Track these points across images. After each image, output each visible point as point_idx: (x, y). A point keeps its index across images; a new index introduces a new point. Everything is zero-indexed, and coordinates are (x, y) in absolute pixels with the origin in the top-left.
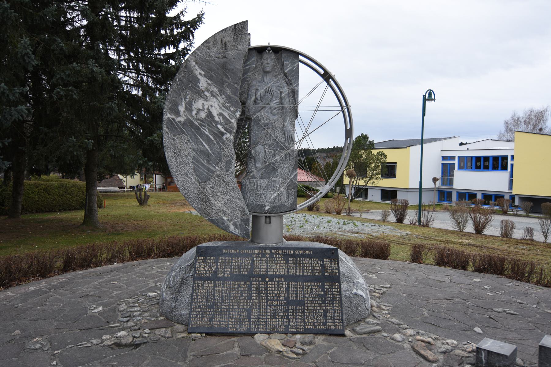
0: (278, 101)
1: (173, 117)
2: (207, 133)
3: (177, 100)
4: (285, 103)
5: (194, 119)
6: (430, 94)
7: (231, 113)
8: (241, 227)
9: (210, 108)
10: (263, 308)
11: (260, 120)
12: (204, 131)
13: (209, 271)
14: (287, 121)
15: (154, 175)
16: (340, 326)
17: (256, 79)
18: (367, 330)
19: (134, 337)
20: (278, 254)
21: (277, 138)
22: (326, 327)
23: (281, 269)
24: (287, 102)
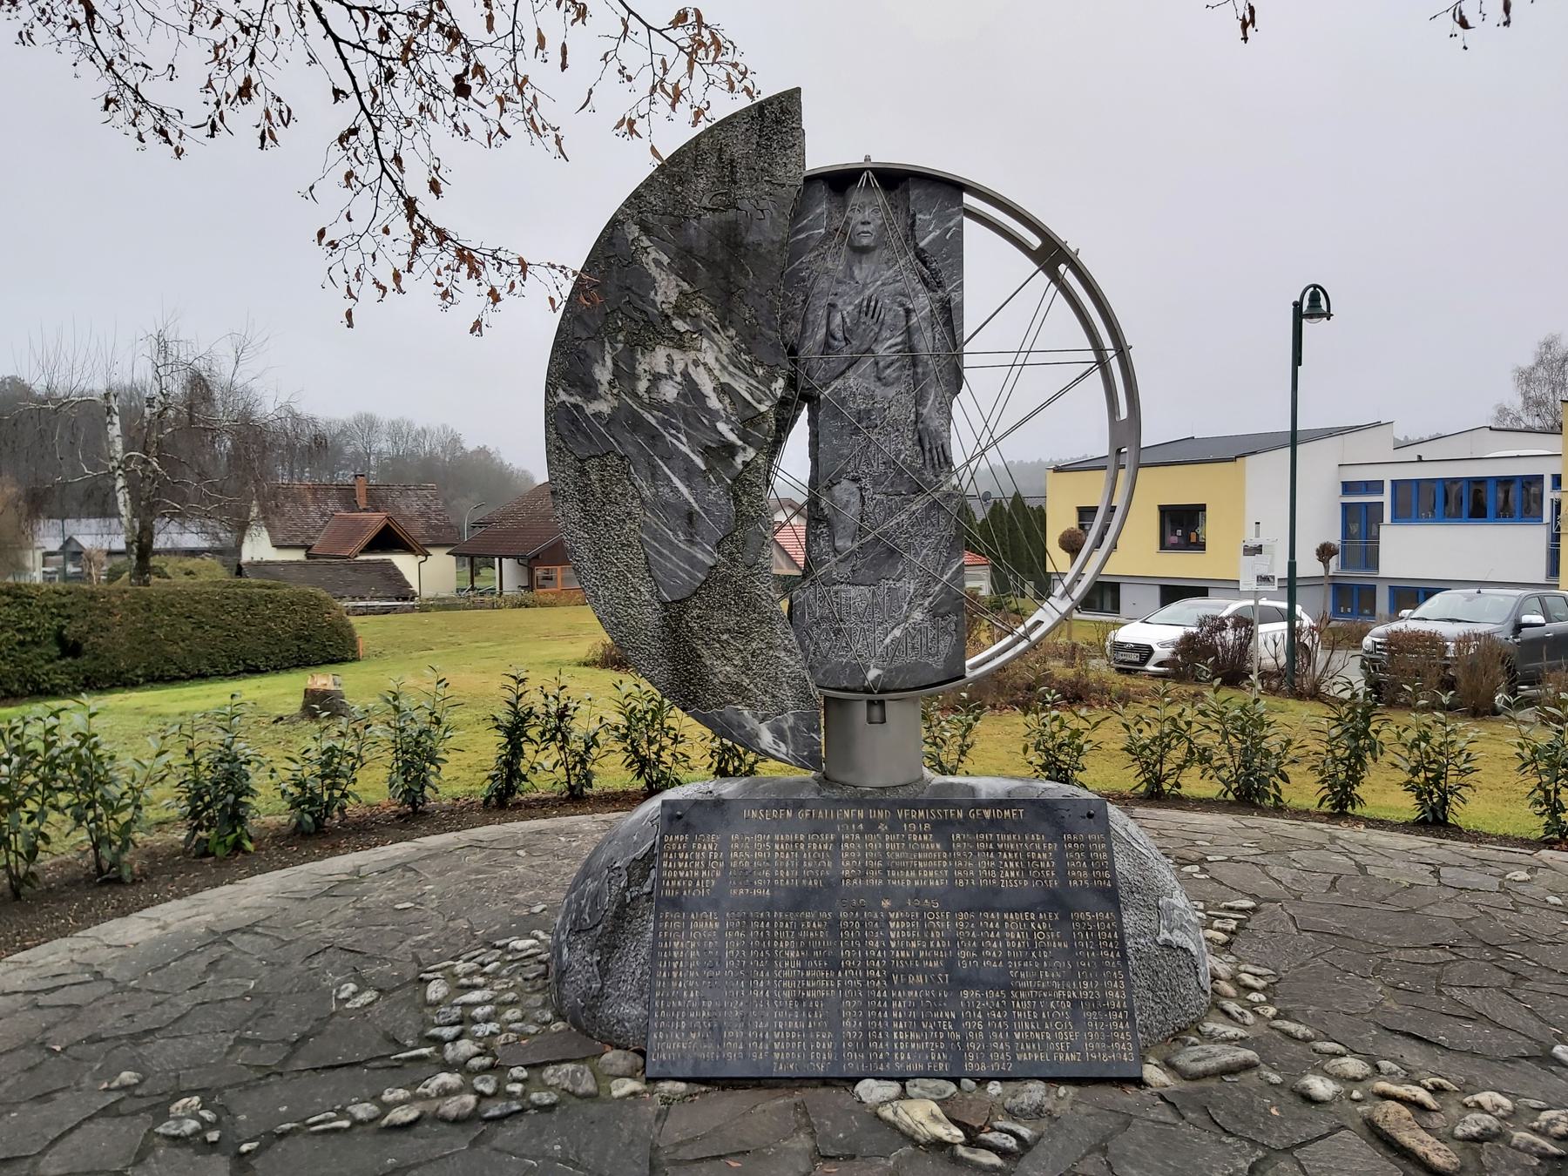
0: (899, 339)
1: (577, 400)
2: (685, 449)
3: (589, 349)
4: (922, 346)
5: (642, 405)
6: (1314, 299)
7: (755, 384)
8: (794, 736)
9: (691, 369)
10: (879, 995)
11: (843, 401)
12: (675, 441)
13: (705, 879)
14: (930, 402)
15: (497, 560)
16: (1127, 1052)
17: (827, 272)
18: (1211, 1064)
19: (482, 1095)
20: (917, 822)
21: (897, 457)
22: (1083, 1055)
23: (928, 869)
24: (926, 342)
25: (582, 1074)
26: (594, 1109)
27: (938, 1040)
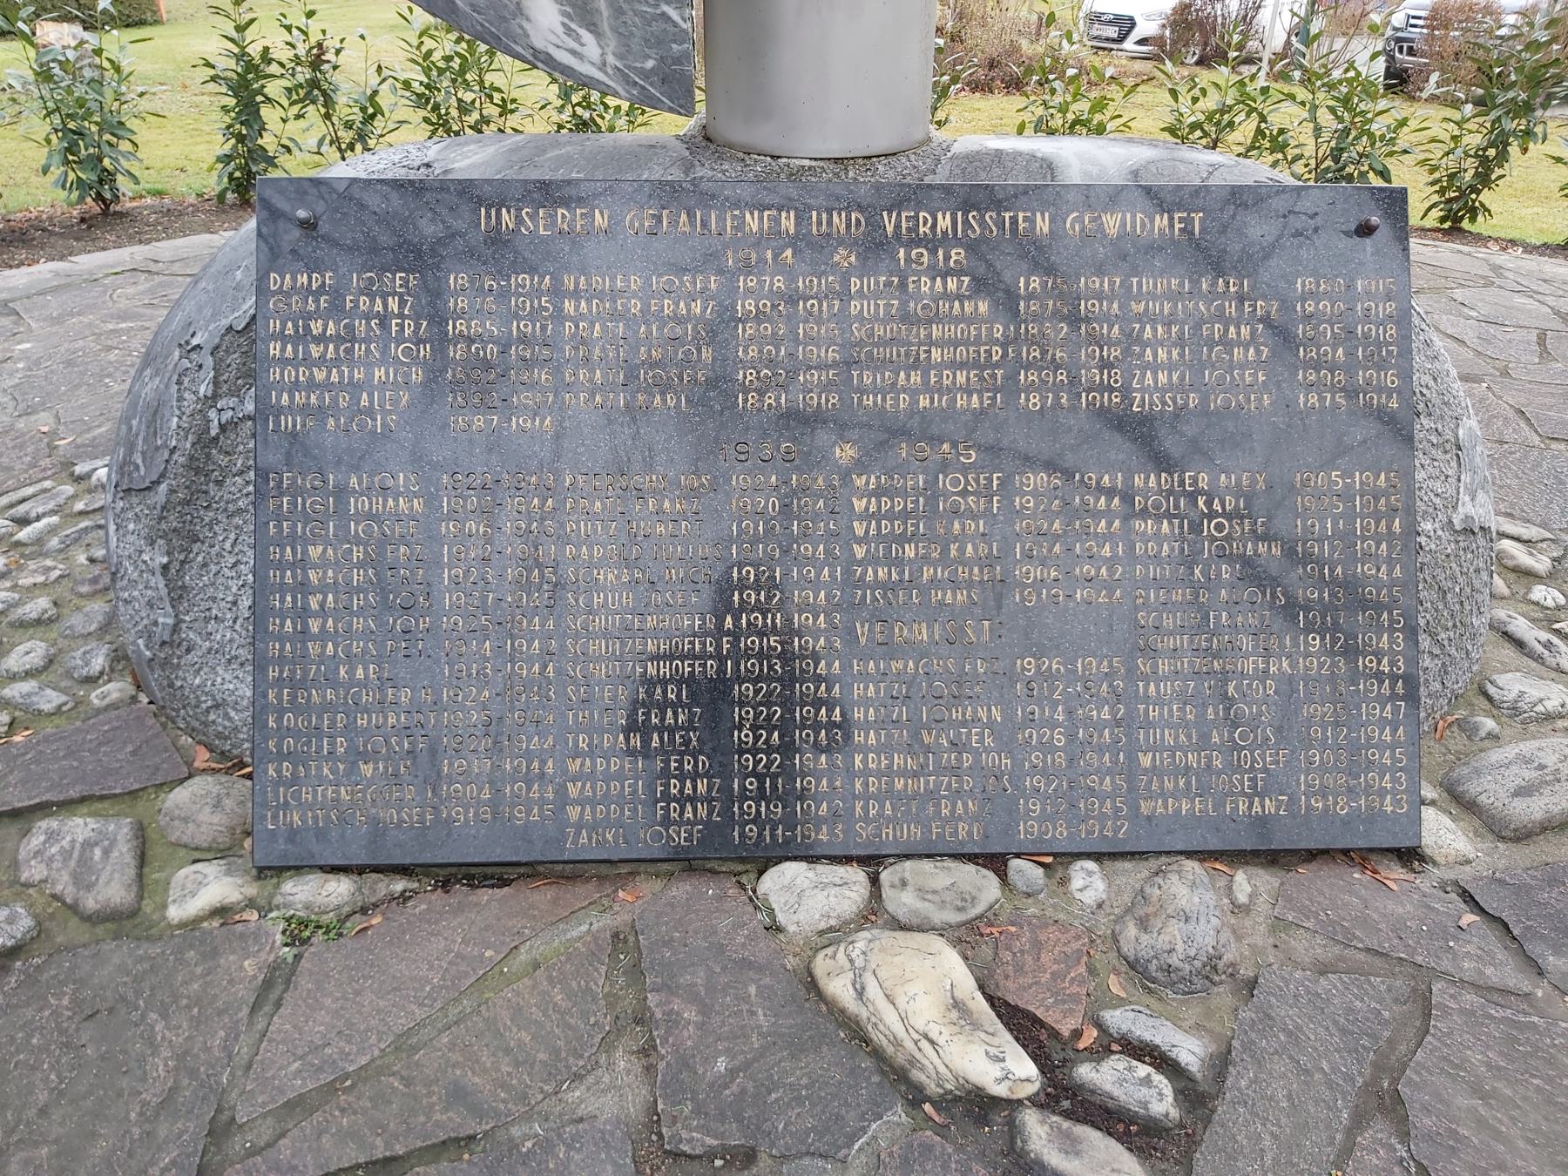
16: (1394, 792)
23: (955, 365)
25: (106, 852)
26: (119, 955)
27: (955, 771)
